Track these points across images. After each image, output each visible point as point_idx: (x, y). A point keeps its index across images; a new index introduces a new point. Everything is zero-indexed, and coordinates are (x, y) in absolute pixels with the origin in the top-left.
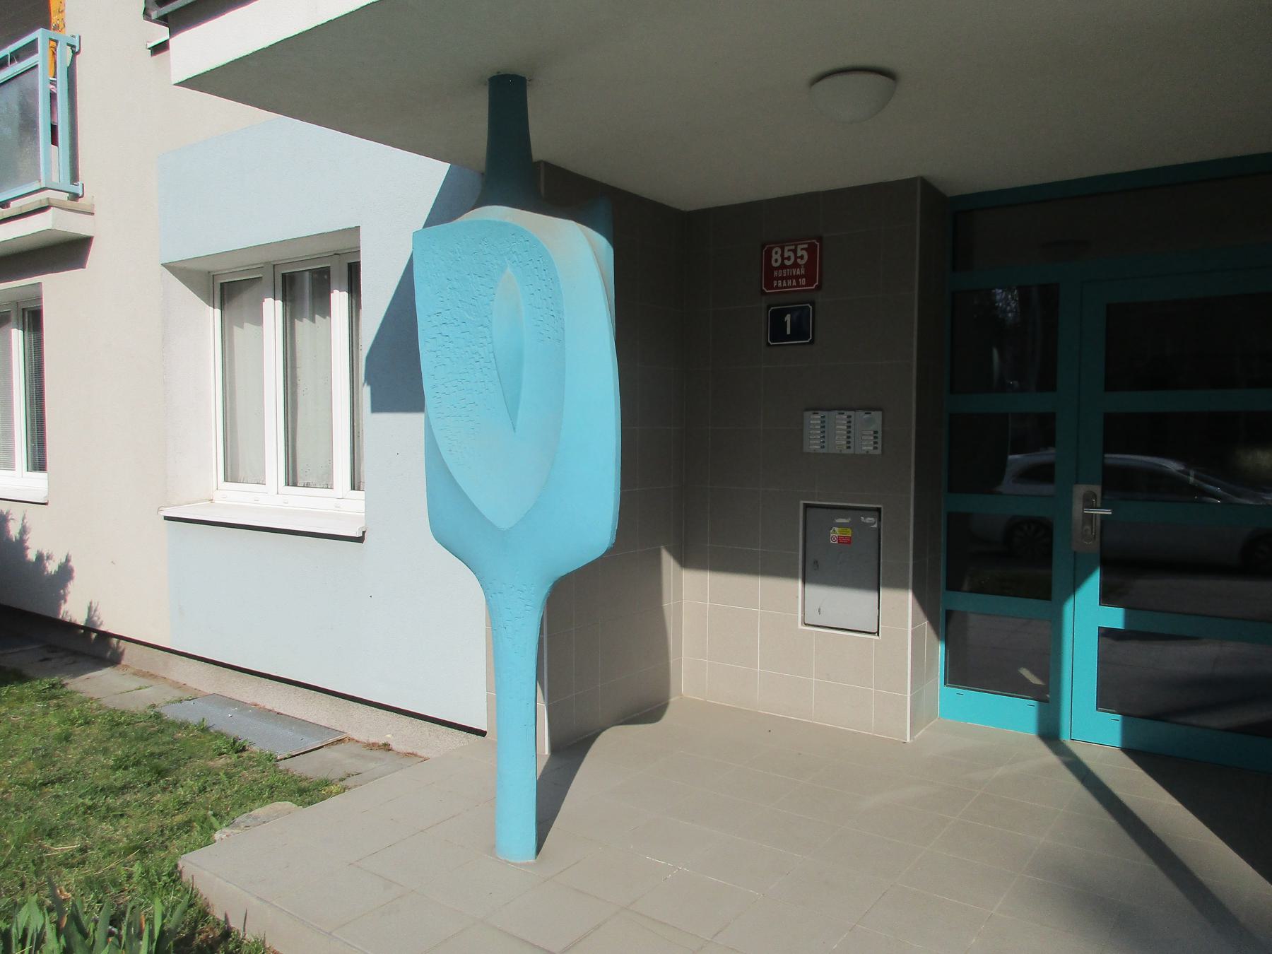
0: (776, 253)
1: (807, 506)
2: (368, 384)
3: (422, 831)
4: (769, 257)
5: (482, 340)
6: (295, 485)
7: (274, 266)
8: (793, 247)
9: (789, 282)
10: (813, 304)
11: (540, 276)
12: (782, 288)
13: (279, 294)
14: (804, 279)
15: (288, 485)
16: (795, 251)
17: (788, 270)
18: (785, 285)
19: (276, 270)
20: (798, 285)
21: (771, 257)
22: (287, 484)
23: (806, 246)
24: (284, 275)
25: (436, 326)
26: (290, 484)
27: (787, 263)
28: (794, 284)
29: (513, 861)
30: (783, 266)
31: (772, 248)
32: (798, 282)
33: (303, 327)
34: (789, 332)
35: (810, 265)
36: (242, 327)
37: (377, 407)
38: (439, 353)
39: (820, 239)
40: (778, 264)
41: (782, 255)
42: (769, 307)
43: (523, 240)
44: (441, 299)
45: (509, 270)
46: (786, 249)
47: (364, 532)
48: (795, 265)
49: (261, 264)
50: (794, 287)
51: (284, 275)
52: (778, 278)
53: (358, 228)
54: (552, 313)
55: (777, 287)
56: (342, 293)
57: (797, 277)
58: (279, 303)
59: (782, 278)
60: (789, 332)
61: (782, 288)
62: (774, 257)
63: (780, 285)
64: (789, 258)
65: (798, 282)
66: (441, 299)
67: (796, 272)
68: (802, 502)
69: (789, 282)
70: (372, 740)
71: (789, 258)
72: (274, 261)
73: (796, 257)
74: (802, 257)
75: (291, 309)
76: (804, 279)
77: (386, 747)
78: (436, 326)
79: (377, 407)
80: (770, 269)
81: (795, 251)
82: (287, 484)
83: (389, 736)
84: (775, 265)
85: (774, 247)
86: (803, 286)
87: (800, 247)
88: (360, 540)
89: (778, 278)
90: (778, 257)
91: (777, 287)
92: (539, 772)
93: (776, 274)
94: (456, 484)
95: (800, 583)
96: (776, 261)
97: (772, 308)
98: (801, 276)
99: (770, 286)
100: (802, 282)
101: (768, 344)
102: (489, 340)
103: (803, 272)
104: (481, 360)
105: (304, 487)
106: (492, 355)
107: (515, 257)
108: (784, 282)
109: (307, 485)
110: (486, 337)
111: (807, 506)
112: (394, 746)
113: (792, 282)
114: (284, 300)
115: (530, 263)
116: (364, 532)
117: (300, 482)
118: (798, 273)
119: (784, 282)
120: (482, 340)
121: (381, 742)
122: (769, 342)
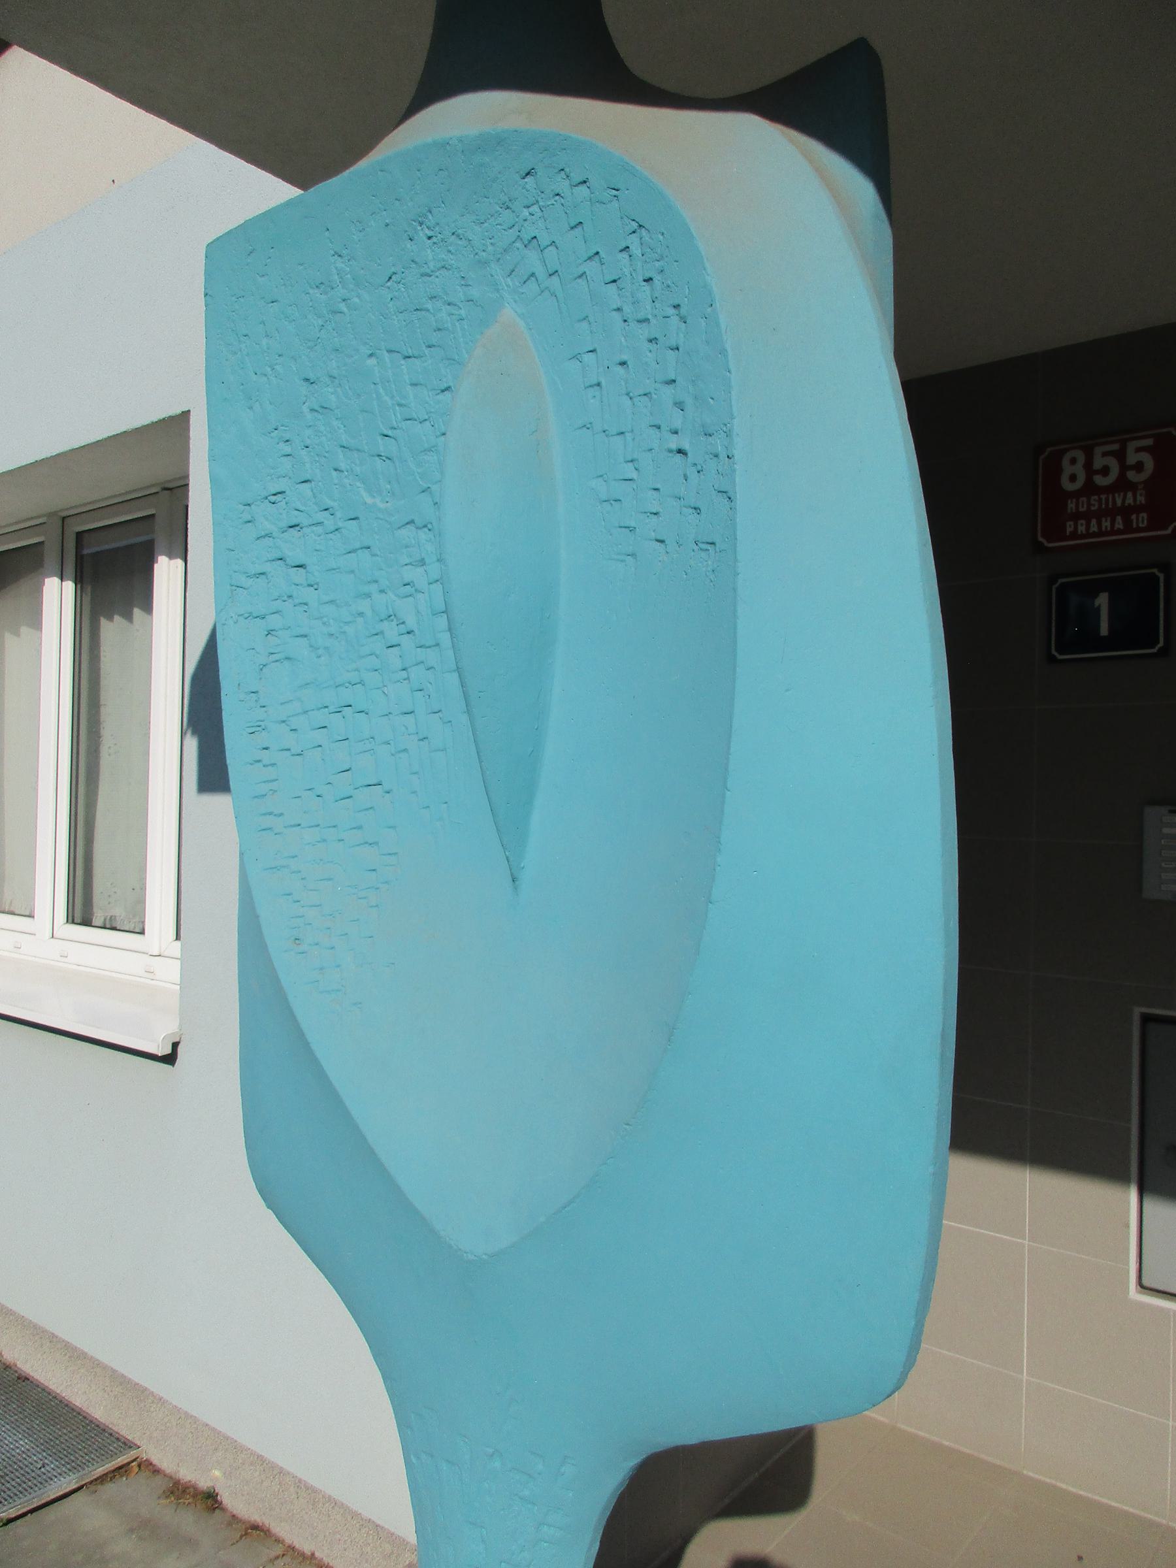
1: (1146, 1019)
2: (194, 733)
4: (1054, 472)
5: (409, 574)
6: (87, 922)
7: (64, 519)
9: (1106, 524)
10: (1165, 567)
11: (627, 309)
12: (1089, 535)
13: (70, 568)
14: (1145, 515)
15: (73, 922)
16: (1120, 455)
17: (1103, 497)
18: (1094, 528)
19: (65, 523)
20: (1128, 528)
21: (1059, 470)
22: (71, 919)
23: (1149, 442)
25: (268, 535)
26: (78, 920)
27: (1100, 480)
30: (1090, 488)
33: (111, 629)
34: (1104, 630)
36: (17, 634)
38: (274, 621)
40: (1078, 485)
41: (1088, 465)
43: (563, 186)
44: (287, 449)
45: (509, 312)
46: (1098, 451)
47: (175, 1045)
48: (1122, 485)
49: (39, 517)
50: (1119, 532)
52: (1076, 516)
53: (189, 411)
54: (674, 443)
55: (1074, 535)
56: (173, 562)
58: (69, 586)
59: (1087, 516)
60: (1104, 630)
62: (1068, 469)
63: (1082, 529)
64: (1105, 471)
66: (287, 449)
67: (1124, 500)
68: (1138, 1011)
69: (1106, 524)
70: (186, 1474)
71: (1105, 471)
72: (61, 510)
73: (1124, 468)
74: (1139, 467)
75: (92, 599)
76: (1145, 515)
77: (210, 1500)
78: (268, 535)
81: (1120, 455)
82: (71, 919)
83: (217, 1473)
84: (1068, 486)
85: (1067, 450)
86: (1139, 530)
87: (1132, 446)
88: (170, 1059)
89: (1076, 516)
90: (1079, 470)
91: (1074, 535)
93: (1071, 506)
94: (314, 1061)
95: (1133, 1195)
96: (1073, 478)
97: (1060, 581)
98: (1137, 509)
100: (1142, 519)
101: (1052, 659)
102: (434, 570)
103: (1141, 499)
104: (406, 640)
105: (104, 928)
106: (442, 621)
107: (532, 257)
108: (1094, 522)
109: (110, 926)
110: (422, 563)
111: (1146, 1019)
112: (226, 1498)
114: (79, 580)
115: (592, 268)
116: (175, 1045)
117: (98, 919)
118: (1130, 500)
119: (1094, 522)
120: (409, 574)
121: (204, 1484)
122: (1054, 652)
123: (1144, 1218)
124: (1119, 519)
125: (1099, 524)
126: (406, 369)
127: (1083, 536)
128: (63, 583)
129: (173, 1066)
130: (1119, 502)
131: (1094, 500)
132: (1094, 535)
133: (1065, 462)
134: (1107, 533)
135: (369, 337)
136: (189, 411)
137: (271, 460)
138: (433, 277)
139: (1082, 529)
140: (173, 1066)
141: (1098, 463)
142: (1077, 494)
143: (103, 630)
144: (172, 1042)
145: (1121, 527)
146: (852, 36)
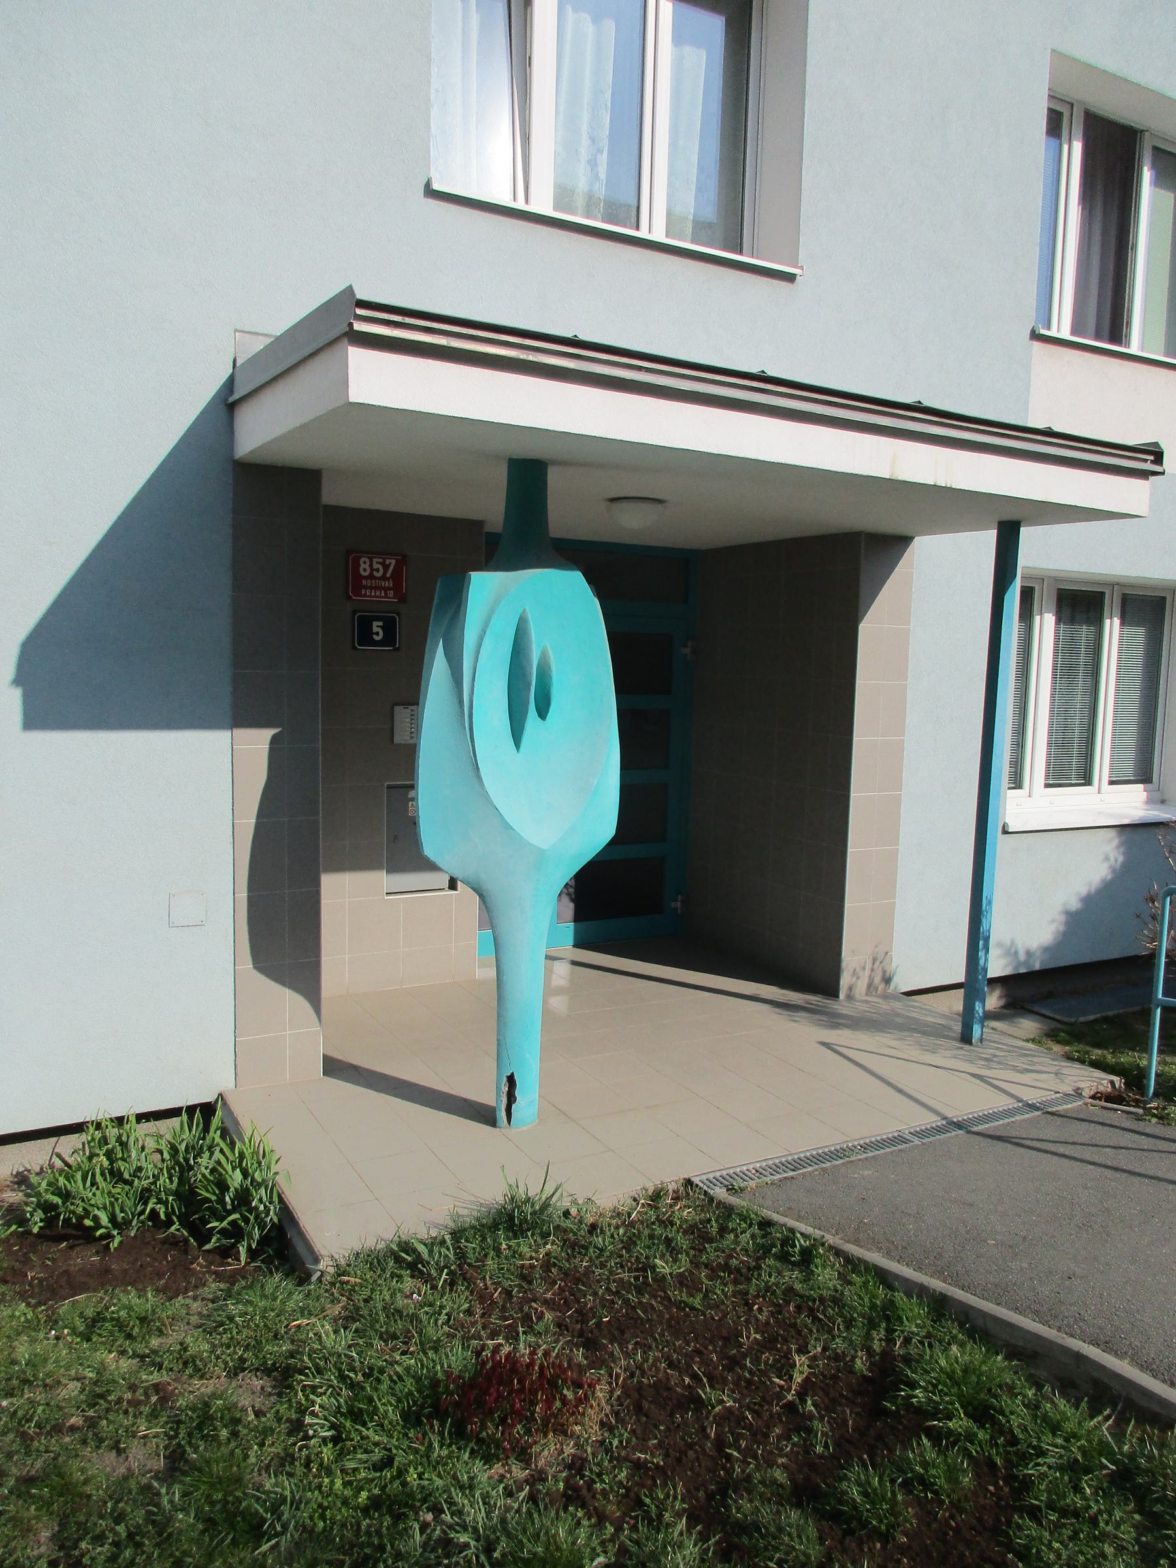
0: (365, 562)
4: (357, 566)
8: (381, 560)
9: (378, 593)
18: (373, 594)
20: (386, 596)
28: (383, 594)
30: (371, 576)
31: (359, 558)
41: (371, 566)
42: (354, 612)
46: (375, 560)
48: (384, 578)
52: (366, 587)
53: (1053, 51)
55: (365, 595)
57: (386, 589)
59: (371, 588)
62: (362, 566)
69: (378, 593)
71: (378, 570)
73: (372, 569)
80: (358, 578)
84: (364, 574)
86: (390, 598)
89: (366, 587)
90: (367, 566)
96: (365, 570)
98: (389, 589)
101: (355, 648)
111: (389, 787)
113: (371, 592)
123: (882, 1084)
127: (368, 597)
128: (1112, 833)
129: (30, 723)
130: (383, 584)
131: (378, 563)
132: (373, 597)
133: (361, 562)
136: (1053, 51)
138: (1086, 1093)
139: (368, 593)
140: (30, 723)
141: (375, 566)
142: (366, 578)
143: (396, 717)
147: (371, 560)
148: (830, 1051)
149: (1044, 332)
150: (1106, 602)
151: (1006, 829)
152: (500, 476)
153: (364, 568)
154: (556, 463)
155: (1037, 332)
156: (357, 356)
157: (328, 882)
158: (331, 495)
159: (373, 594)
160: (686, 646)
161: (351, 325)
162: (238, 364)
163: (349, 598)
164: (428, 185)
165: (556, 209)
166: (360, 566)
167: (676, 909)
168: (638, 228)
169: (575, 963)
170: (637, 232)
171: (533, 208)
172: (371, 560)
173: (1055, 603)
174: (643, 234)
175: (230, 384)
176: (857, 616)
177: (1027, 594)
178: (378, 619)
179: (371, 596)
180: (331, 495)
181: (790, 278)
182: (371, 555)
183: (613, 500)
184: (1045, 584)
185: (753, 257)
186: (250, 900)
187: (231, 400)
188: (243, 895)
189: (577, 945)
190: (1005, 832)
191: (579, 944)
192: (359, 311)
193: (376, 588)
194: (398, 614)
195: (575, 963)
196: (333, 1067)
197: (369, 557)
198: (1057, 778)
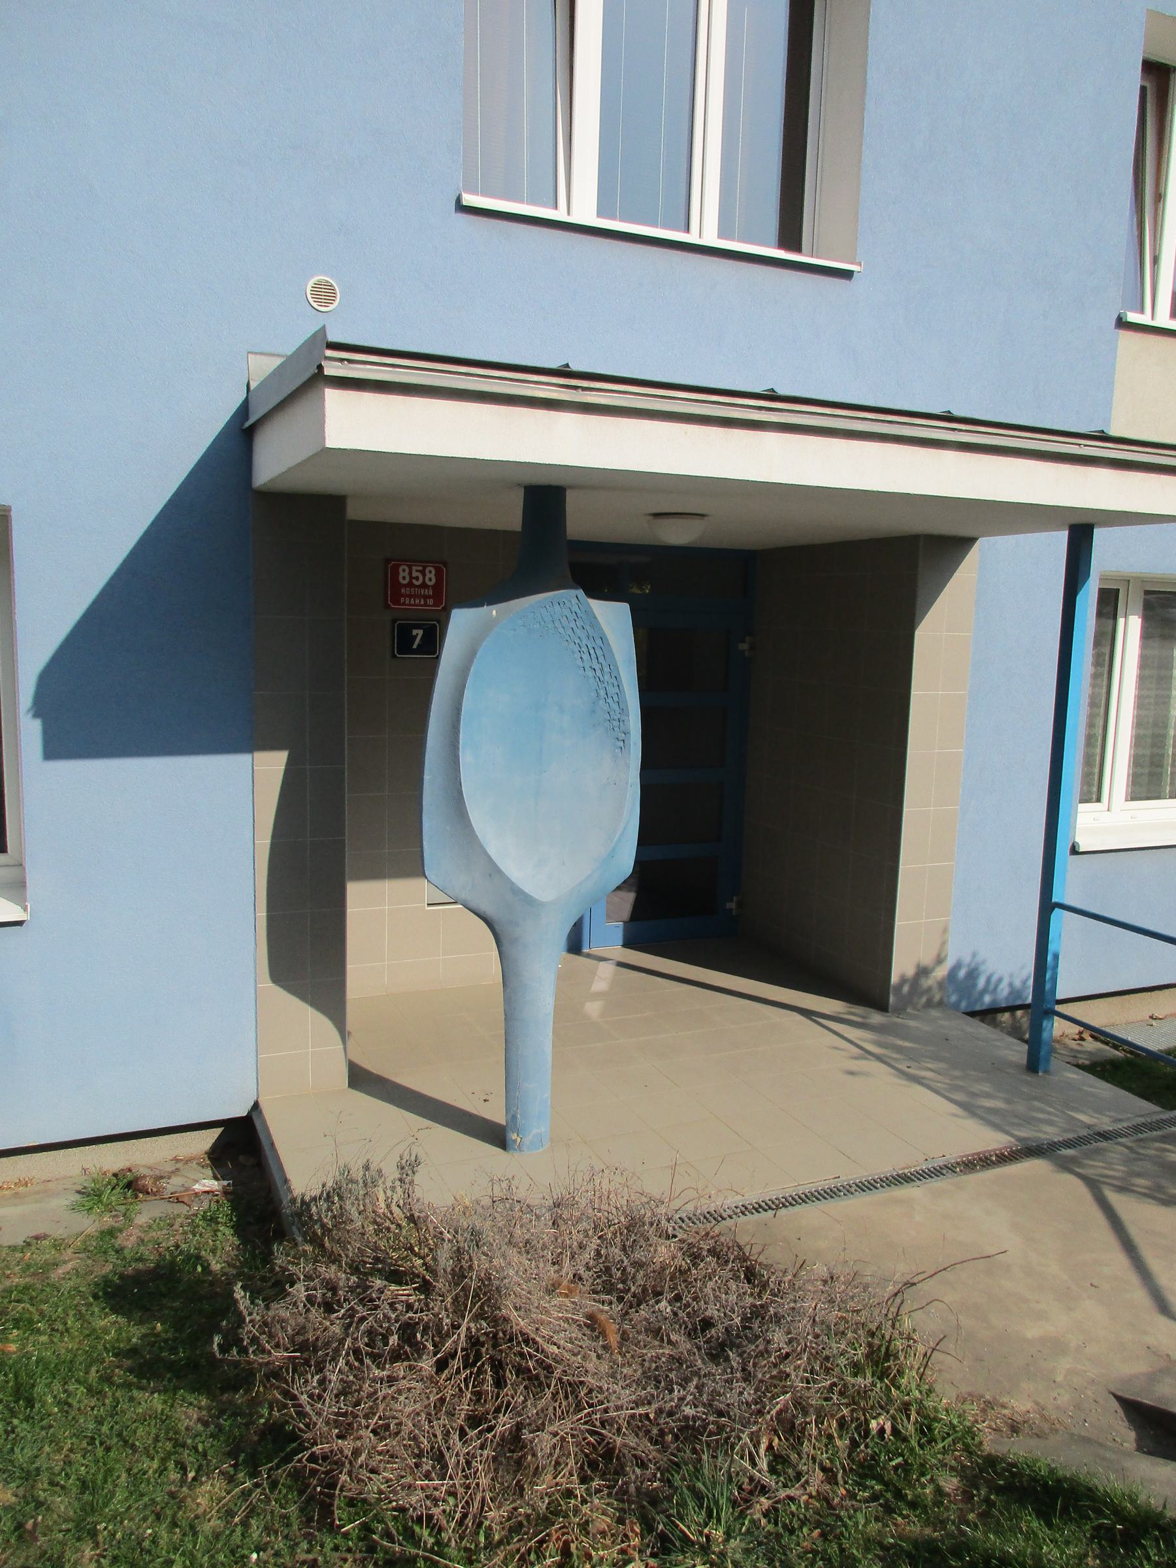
0: (404, 571)
3: (678, 1210)
8: (420, 568)
9: (417, 601)
16: (423, 573)
18: (412, 602)
20: (426, 605)
21: (398, 573)
24: (1099, 800)
28: (422, 602)
29: (734, 1200)
30: (410, 584)
31: (399, 566)
32: (425, 602)
34: (415, 646)
35: (437, 587)
37: (54, 750)
39: (445, 564)
41: (410, 573)
42: (394, 621)
46: (414, 568)
48: (424, 585)
50: (422, 606)
51: (1099, 800)
52: (405, 596)
55: (404, 604)
57: (426, 597)
59: (410, 596)
60: (415, 646)
61: (415, 605)
62: (402, 574)
65: (425, 602)
69: (417, 601)
71: (417, 578)
79: (54, 750)
80: (396, 585)
81: (423, 573)
85: (401, 565)
86: (430, 606)
89: (405, 596)
90: (406, 574)
92: (1103, 1029)
96: (404, 578)
99: (397, 602)
101: (394, 656)
103: (431, 593)
113: (410, 600)
118: (426, 593)
122: (398, 622)
124: (422, 600)
125: (415, 600)
126: (177, 1358)
131: (417, 571)
134: (417, 605)
135: (327, 1244)
137: (203, 1360)
139: (407, 602)
141: (415, 574)
142: (405, 586)
144: (564, 953)
145: (415, 632)
146: (351, 1090)
147: (410, 567)
148: (883, 1065)
149: (1133, 317)
150: (1148, 119)
151: (1077, 850)
152: (517, 500)
153: (403, 575)
154: (571, 487)
155: (1124, 320)
156: (333, 397)
157: (354, 890)
158: (354, 512)
159: (412, 602)
160: (743, 641)
161: (320, 367)
162: (252, 388)
163: (387, 607)
164: (459, 200)
165: (600, 214)
166: (399, 573)
167: (731, 910)
168: (688, 230)
169: (621, 964)
170: (686, 235)
171: (575, 219)
172: (410, 567)
173: (1142, 604)
174: (691, 238)
175: (244, 410)
176: (914, 622)
177: (1109, 602)
178: (418, 627)
179: (410, 605)
180: (354, 512)
181: (847, 275)
182: (410, 562)
183: (657, 515)
184: (1131, 585)
185: (812, 256)
186: (270, 919)
187: (247, 424)
188: (262, 914)
189: (629, 943)
190: (1074, 851)
191: (629, 943)
192: (329, 353)
193: (415, 596)
194: (439, 622)
195: (621, 964)
196: (359, 1078)
197: (408, 566)
198: (1136, 794)
